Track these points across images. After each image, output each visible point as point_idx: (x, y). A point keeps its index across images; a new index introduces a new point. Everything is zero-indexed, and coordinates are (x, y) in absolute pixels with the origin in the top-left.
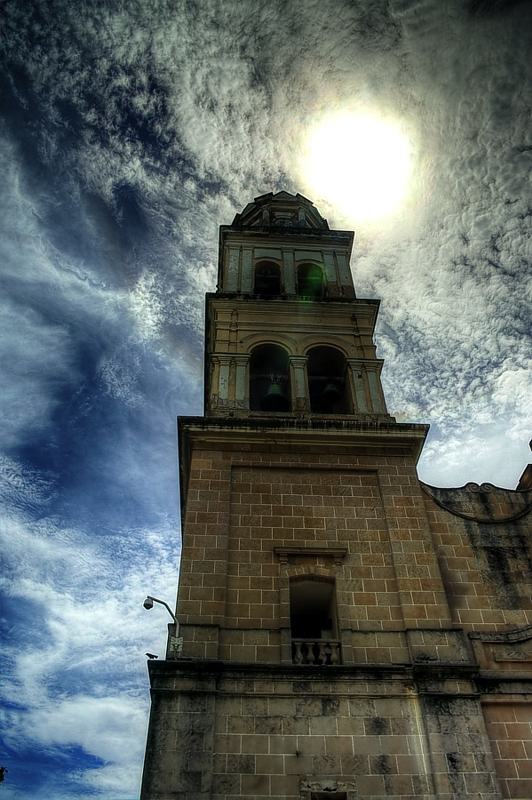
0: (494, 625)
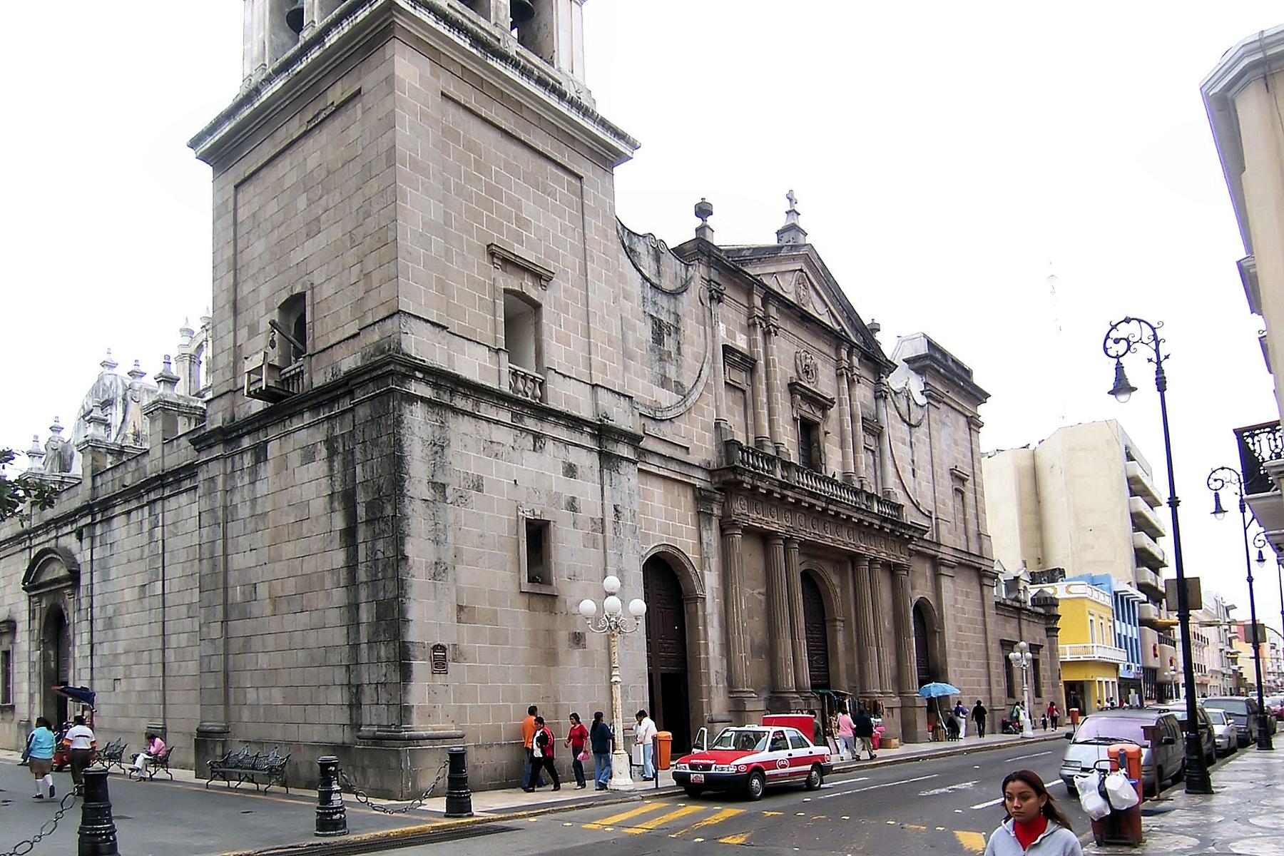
0: (647, 399)
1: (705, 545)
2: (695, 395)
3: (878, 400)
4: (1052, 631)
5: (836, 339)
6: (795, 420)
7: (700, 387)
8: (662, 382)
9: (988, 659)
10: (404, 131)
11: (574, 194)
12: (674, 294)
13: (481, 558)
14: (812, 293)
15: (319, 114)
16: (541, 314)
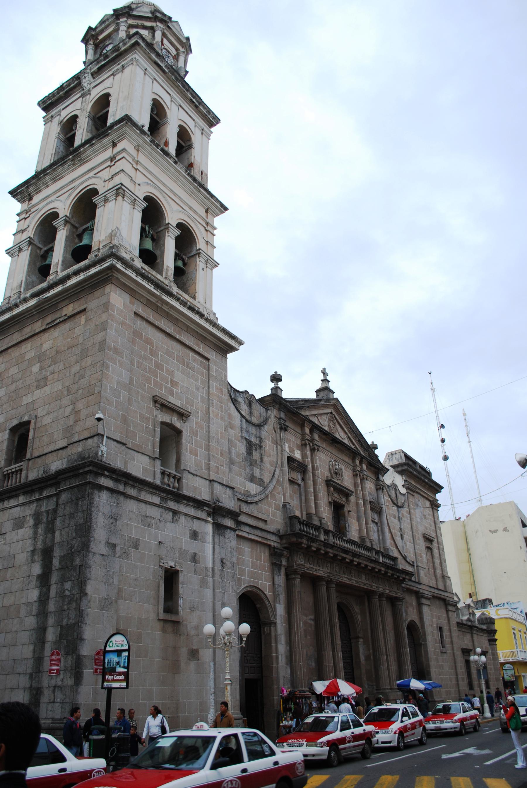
1: (276, 586)
2: (271, 487)
3: (378, 491)
4: (493, 641)
5: (353, 454)
6: (330, 503)
7: (274, 482)
8: (251, 479)
9: (455, 662)
10: (112, 332)
11: (204, 368)
12: (259, 426)
13: (134, 595)
14: (338, 426)
15: (55, 320)
16: (182, 436)
